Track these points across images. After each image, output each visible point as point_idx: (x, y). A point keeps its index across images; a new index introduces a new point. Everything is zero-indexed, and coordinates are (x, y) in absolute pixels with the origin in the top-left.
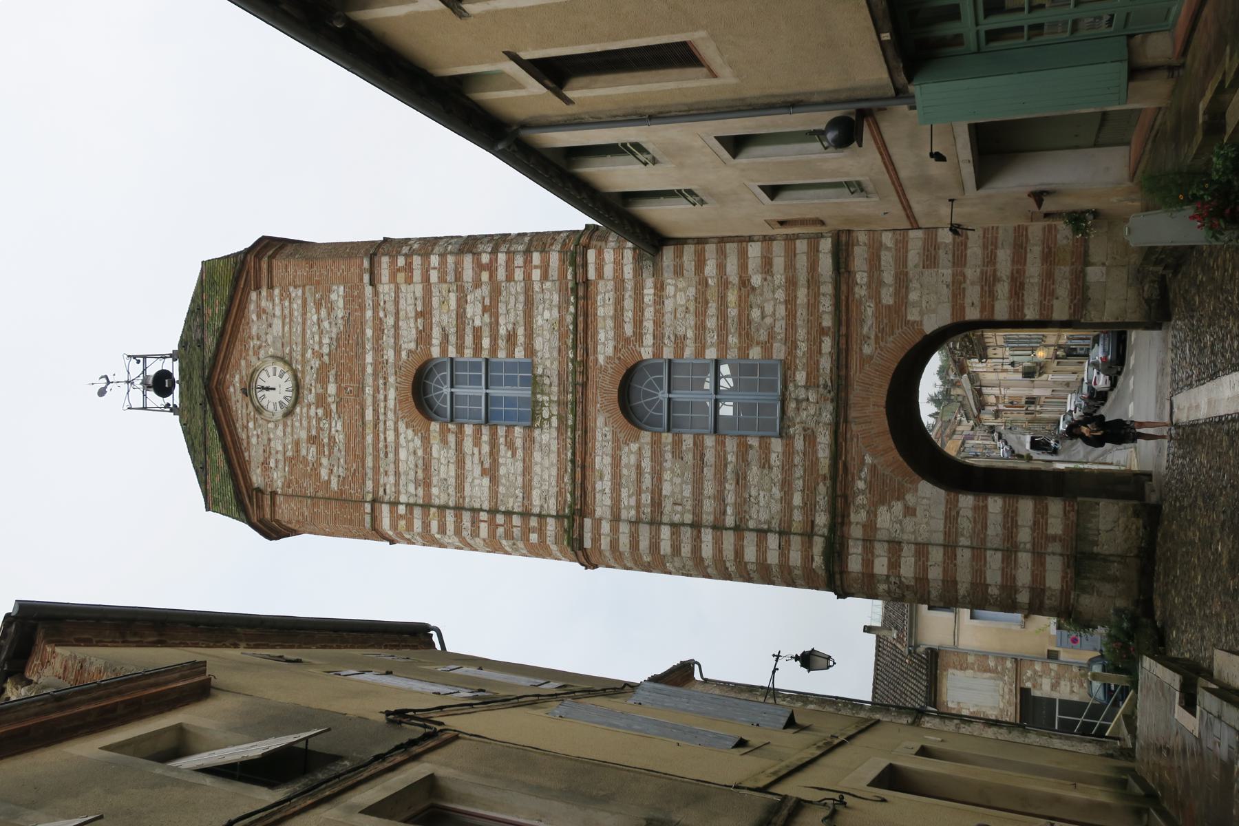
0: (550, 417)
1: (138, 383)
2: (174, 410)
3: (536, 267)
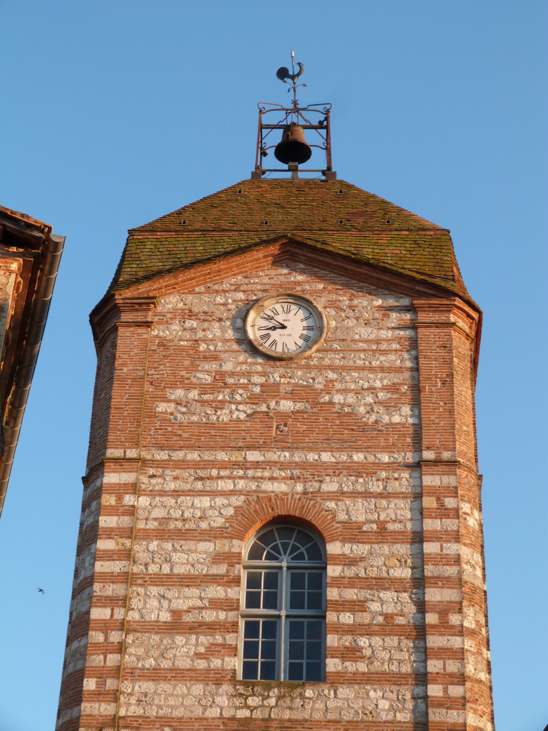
0: (247, 707)
1: (293, 118)
2: (258, 173)
3: (446, 690)
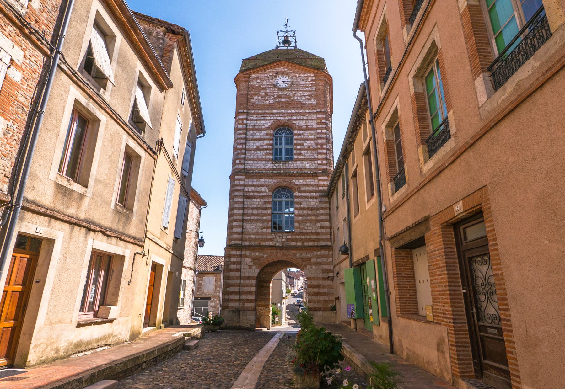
1: (286, 34)
2: (277, 47)
